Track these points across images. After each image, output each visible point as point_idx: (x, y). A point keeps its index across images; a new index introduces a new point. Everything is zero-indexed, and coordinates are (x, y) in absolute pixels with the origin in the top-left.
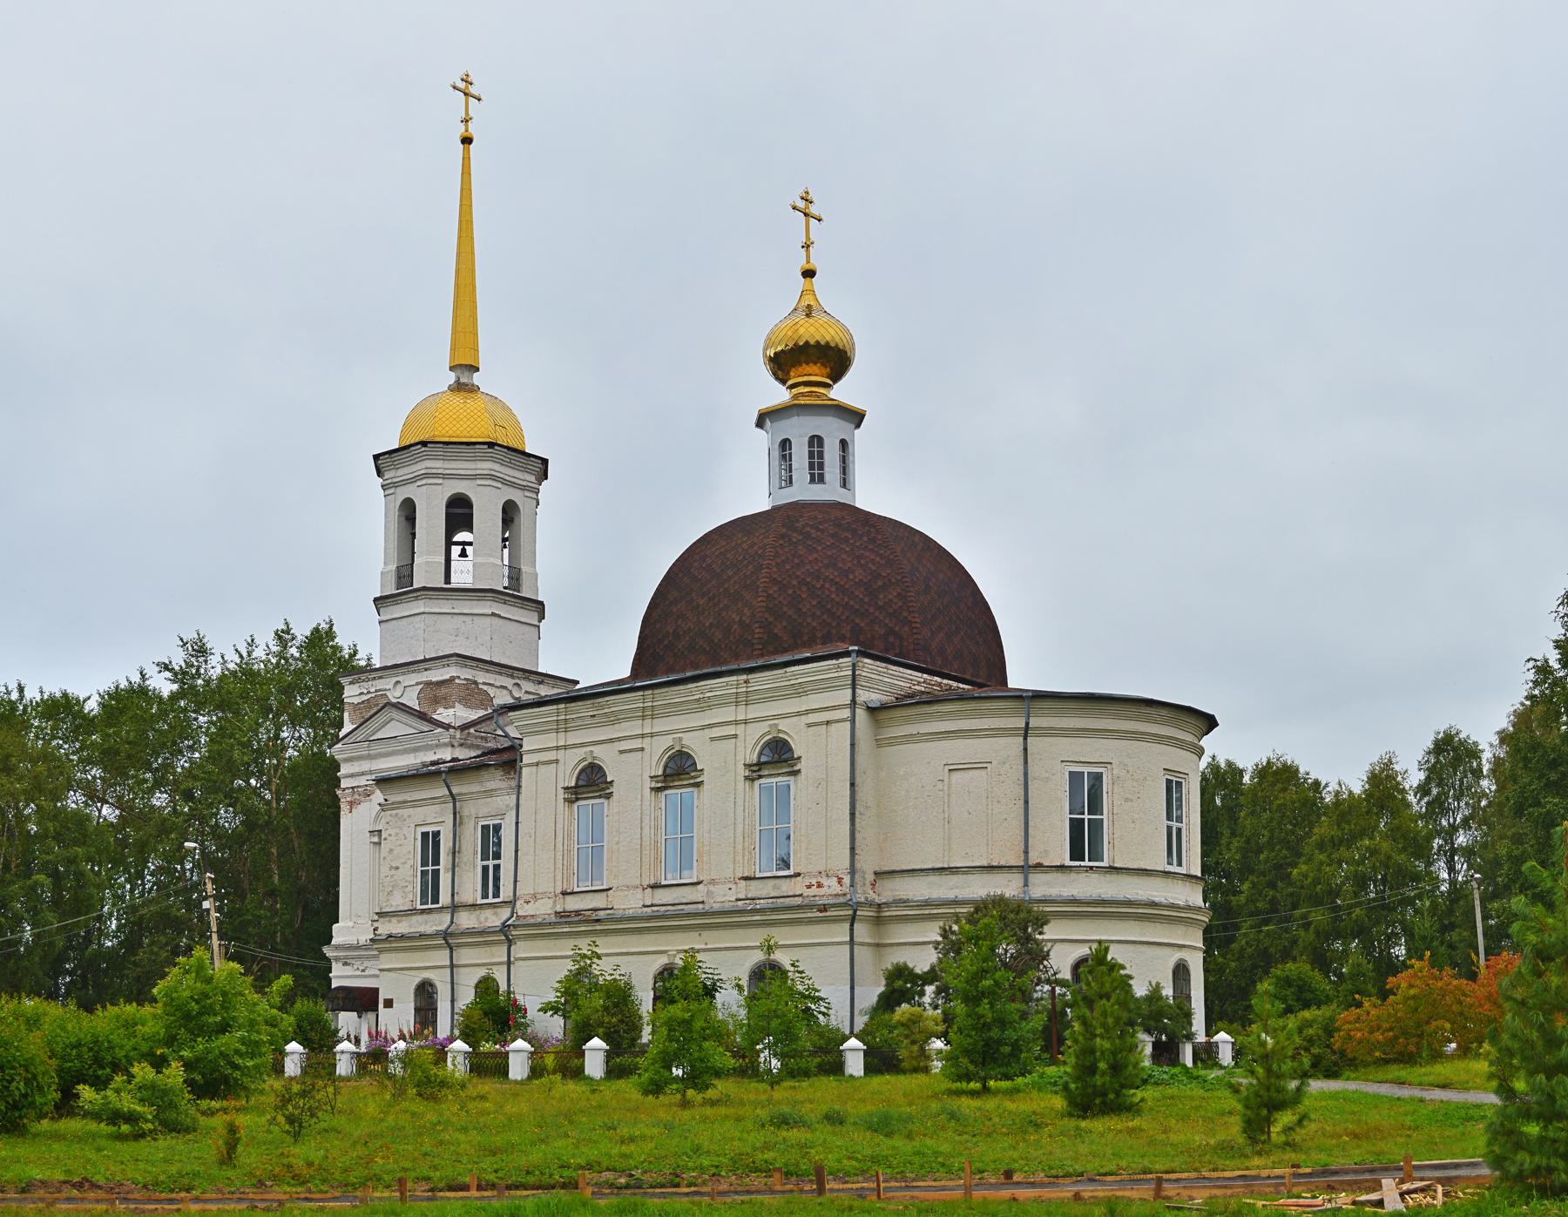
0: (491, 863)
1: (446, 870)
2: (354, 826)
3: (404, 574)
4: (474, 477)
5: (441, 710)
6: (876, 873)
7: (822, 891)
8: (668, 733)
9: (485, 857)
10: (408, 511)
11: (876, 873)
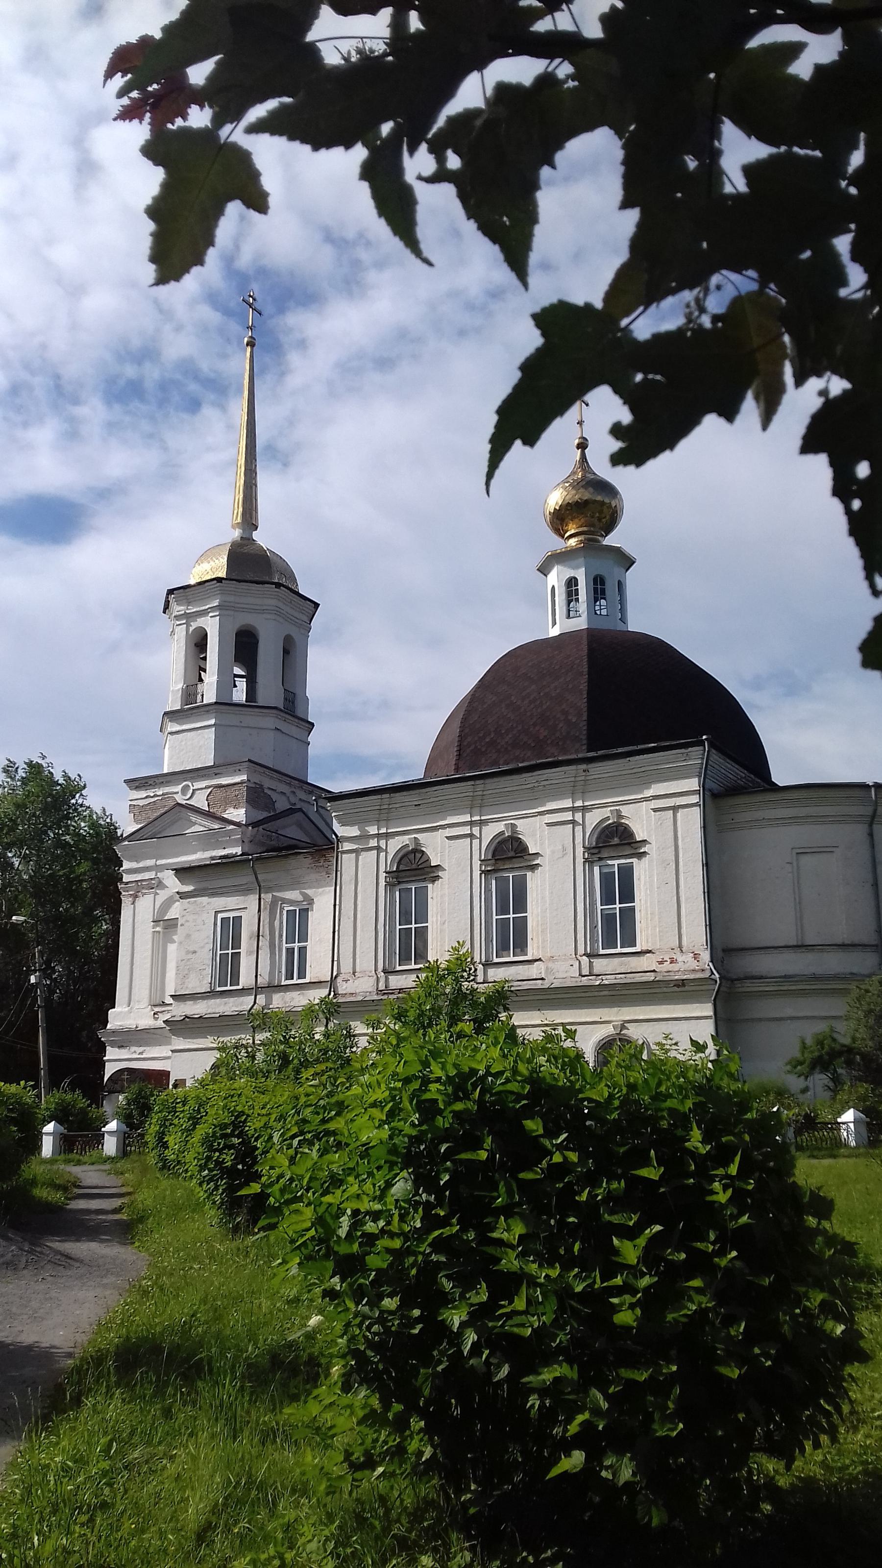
0: (296, 945)
1: (249, 953)
2: (136, 919)
3: (190, 694)
4: (263, 611)
5: (231, 810)
6: (724, 951)
7: (675, 967)
8: (498, 820)
9: (290, 939)
10: (199, 643)
11: (724, 951)
